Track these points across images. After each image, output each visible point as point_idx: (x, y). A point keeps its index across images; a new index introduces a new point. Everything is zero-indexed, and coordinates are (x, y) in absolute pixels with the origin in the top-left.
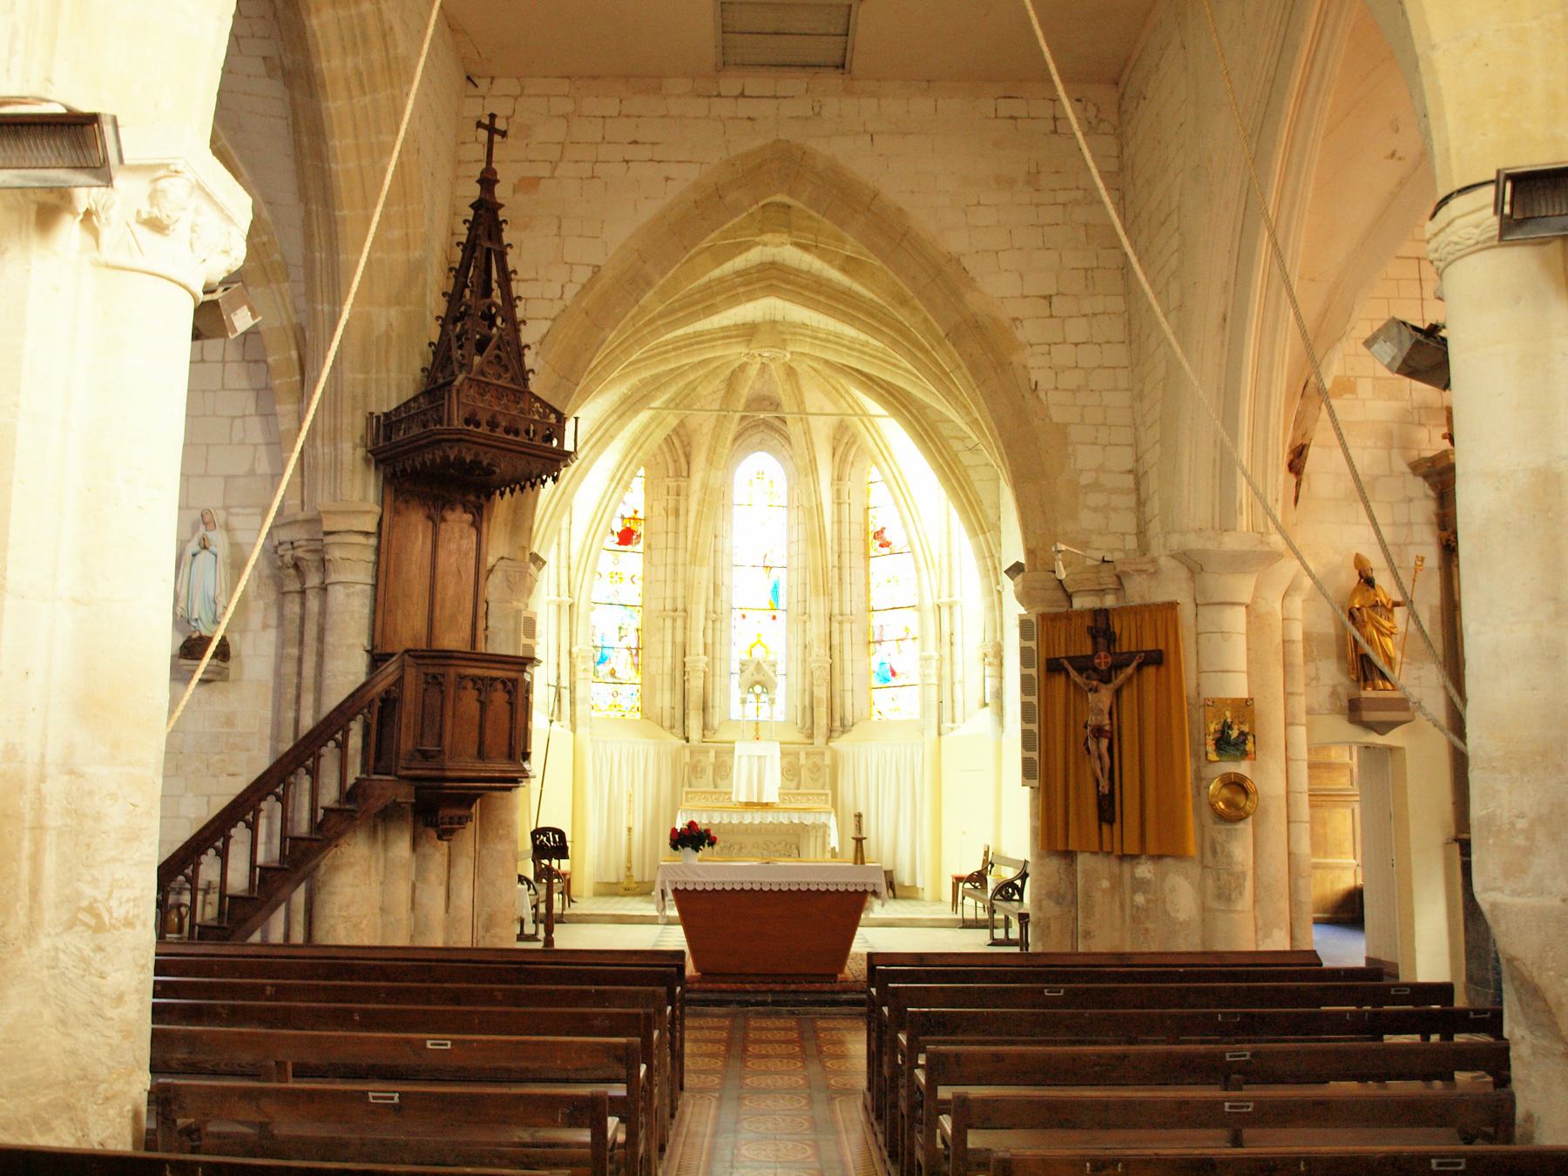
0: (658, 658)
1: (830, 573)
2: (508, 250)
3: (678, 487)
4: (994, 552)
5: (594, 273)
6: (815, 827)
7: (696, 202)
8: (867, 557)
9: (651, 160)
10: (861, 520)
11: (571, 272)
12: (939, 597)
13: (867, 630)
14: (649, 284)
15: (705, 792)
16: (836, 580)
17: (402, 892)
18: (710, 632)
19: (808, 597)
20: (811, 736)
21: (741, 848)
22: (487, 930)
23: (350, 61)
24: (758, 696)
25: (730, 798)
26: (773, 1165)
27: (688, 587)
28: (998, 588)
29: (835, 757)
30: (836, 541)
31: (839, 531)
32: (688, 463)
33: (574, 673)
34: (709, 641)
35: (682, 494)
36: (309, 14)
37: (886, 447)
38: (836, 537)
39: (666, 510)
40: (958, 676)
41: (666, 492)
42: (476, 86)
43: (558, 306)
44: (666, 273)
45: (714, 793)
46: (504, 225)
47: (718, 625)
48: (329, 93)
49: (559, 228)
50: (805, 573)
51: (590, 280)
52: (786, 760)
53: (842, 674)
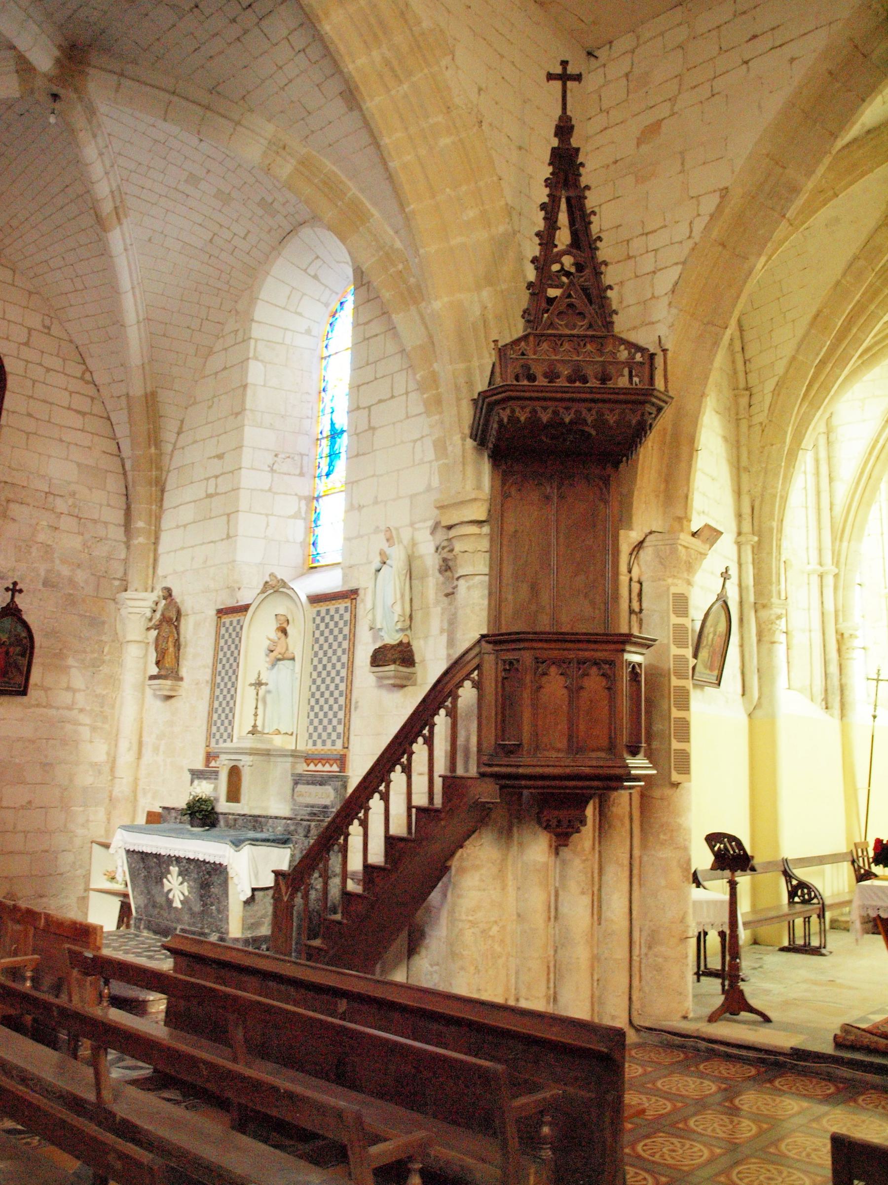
2: (587, 193)
5: (722, 197)
7: (830, 73)
11: (698, 205)
14: (795, 190)
17: (537, 899)
22: (650, 948)
23: (375, 53)
36: (320, 22)
42: (596, 57)
43: (690, 244)
44: (814, 172)
46: (581, 169)
48: (365, 94)
49: (682, 164)
51: (718, 206)
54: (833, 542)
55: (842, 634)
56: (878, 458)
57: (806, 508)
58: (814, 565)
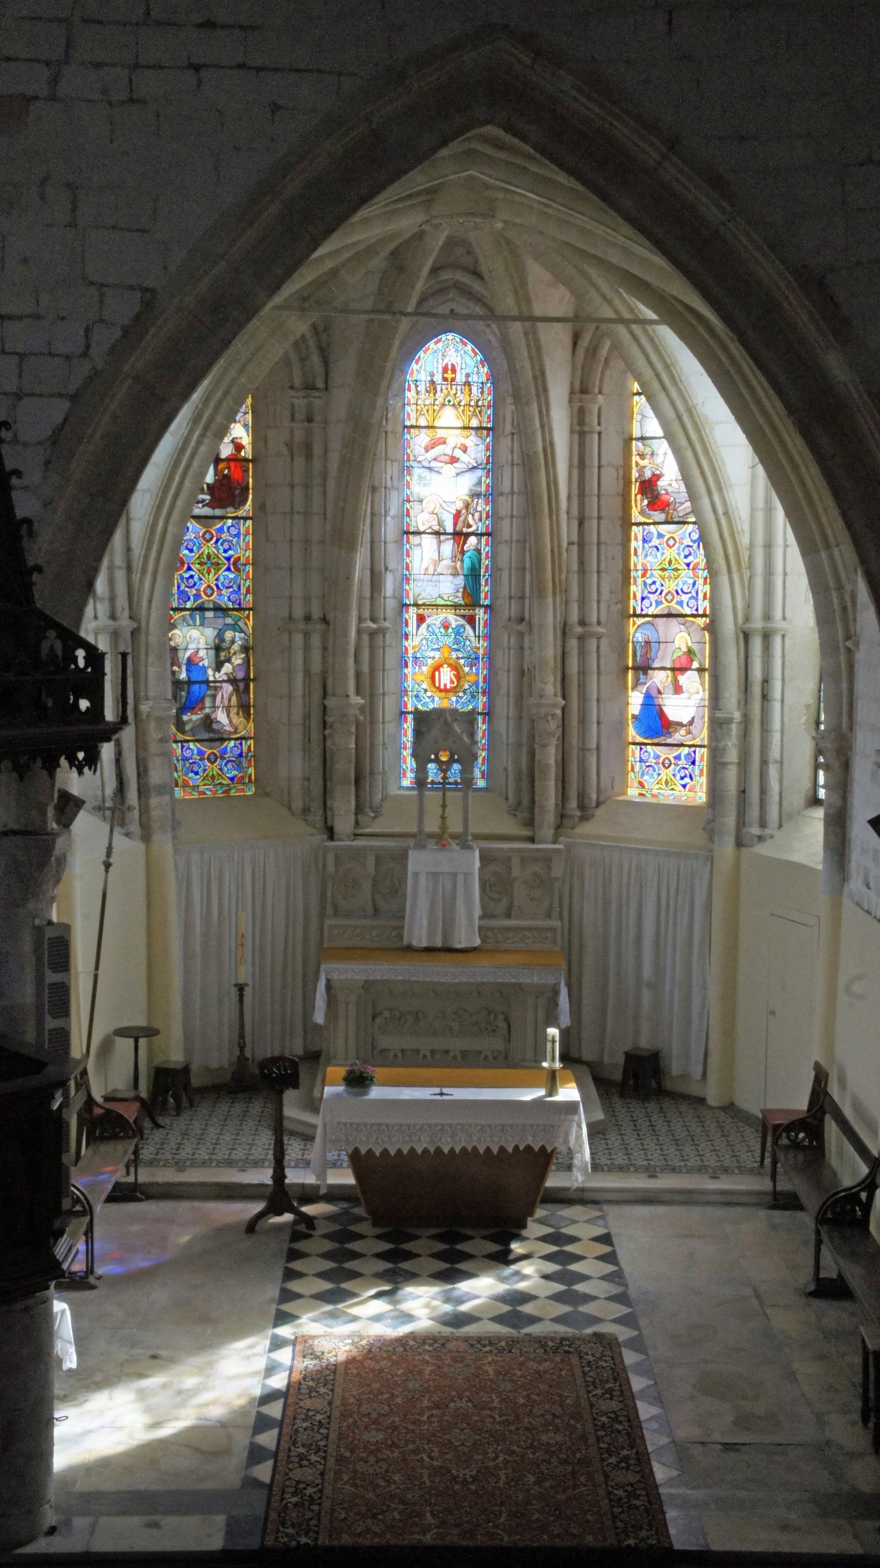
0: (282, 697)
8: (626, 524)
9: (241, 66)
10: (618, 460)
16: (575, 566)
18: (365, 654)
26: (454, 387)
28: (849, 644)
32: (326, 362)
35: (318, 418)
37: (667, 367)
38: (575, 491)
39: (289, 446)
40: (775, 752)
43: (82, 370)
51: (137, 318)
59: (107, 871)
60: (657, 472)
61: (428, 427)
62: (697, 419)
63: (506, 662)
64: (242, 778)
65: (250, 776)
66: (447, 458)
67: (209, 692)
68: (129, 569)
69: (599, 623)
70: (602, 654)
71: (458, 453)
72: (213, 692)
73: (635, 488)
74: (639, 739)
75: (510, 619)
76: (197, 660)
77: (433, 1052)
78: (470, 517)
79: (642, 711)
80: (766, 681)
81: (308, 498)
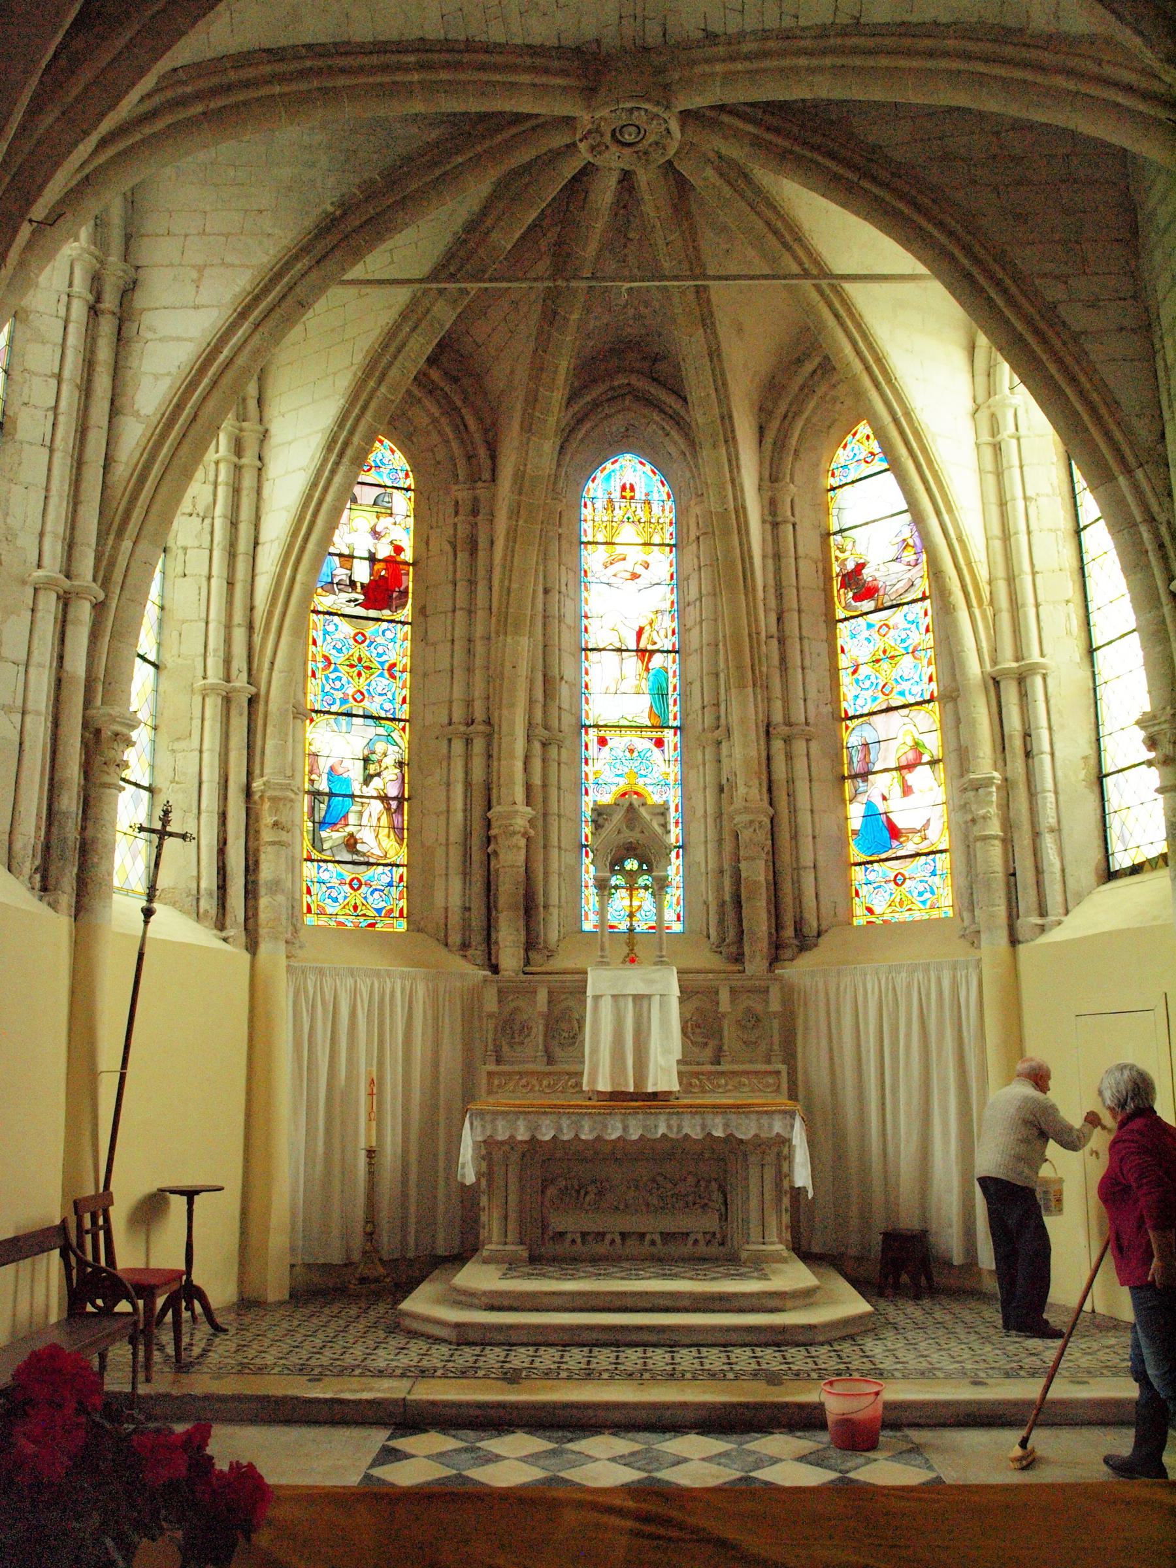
1: (764, 648)
3: (476, 500)
4: (1155, 508)
6: (760, 1145)
8: (832, 622)
10: (817, 554)
12: (994, 662)
13: (836, 750)
15: (527, 1073)
18: (537, 764)
19: (722, 697)
20: (738, 958)
21: (600, 1193)
24: (631, 876)
25: (579, 1084)
27: (495, 677)
29: (789, 995)
30: (771, 591)
31: (778, 572)
32: (493, 458)
33: (257, 832)
34: (537, 781)
37: (879, 360)
40: (1048, 817)
41: (451, 510)
45: (550, 1074)
47: (553, 752)
50: (717, 652)
52: (694, 1004)
53: (795, 837)
54: (101, 536)
55: (98, 732)
56: (215, 383)
57: (52, 451)
58: (52, 567)
59: (146, 922)
60: (862, 561)
61: (606, 543)
62: (916, 424)
63: (702, 780)
64: (392, 911)
65: (401, 910)
66: (628, 575)
67: (354, 808)
68: (251, 627)
69: (807, 724)
70: (812, 757)
71: (639, 570)
72: (360, 808)
73: (836, 584)
74: (863, 858)
75: (704, 730)
76: (340, 770)
77: (623, 1235)
78: (654, 634)
79: (865, 825)
80: (1027, 735)
81: (472, 593)
